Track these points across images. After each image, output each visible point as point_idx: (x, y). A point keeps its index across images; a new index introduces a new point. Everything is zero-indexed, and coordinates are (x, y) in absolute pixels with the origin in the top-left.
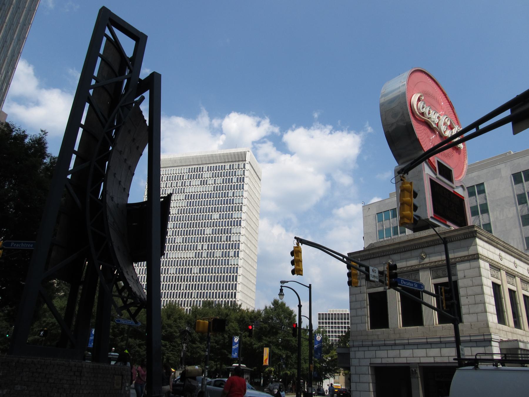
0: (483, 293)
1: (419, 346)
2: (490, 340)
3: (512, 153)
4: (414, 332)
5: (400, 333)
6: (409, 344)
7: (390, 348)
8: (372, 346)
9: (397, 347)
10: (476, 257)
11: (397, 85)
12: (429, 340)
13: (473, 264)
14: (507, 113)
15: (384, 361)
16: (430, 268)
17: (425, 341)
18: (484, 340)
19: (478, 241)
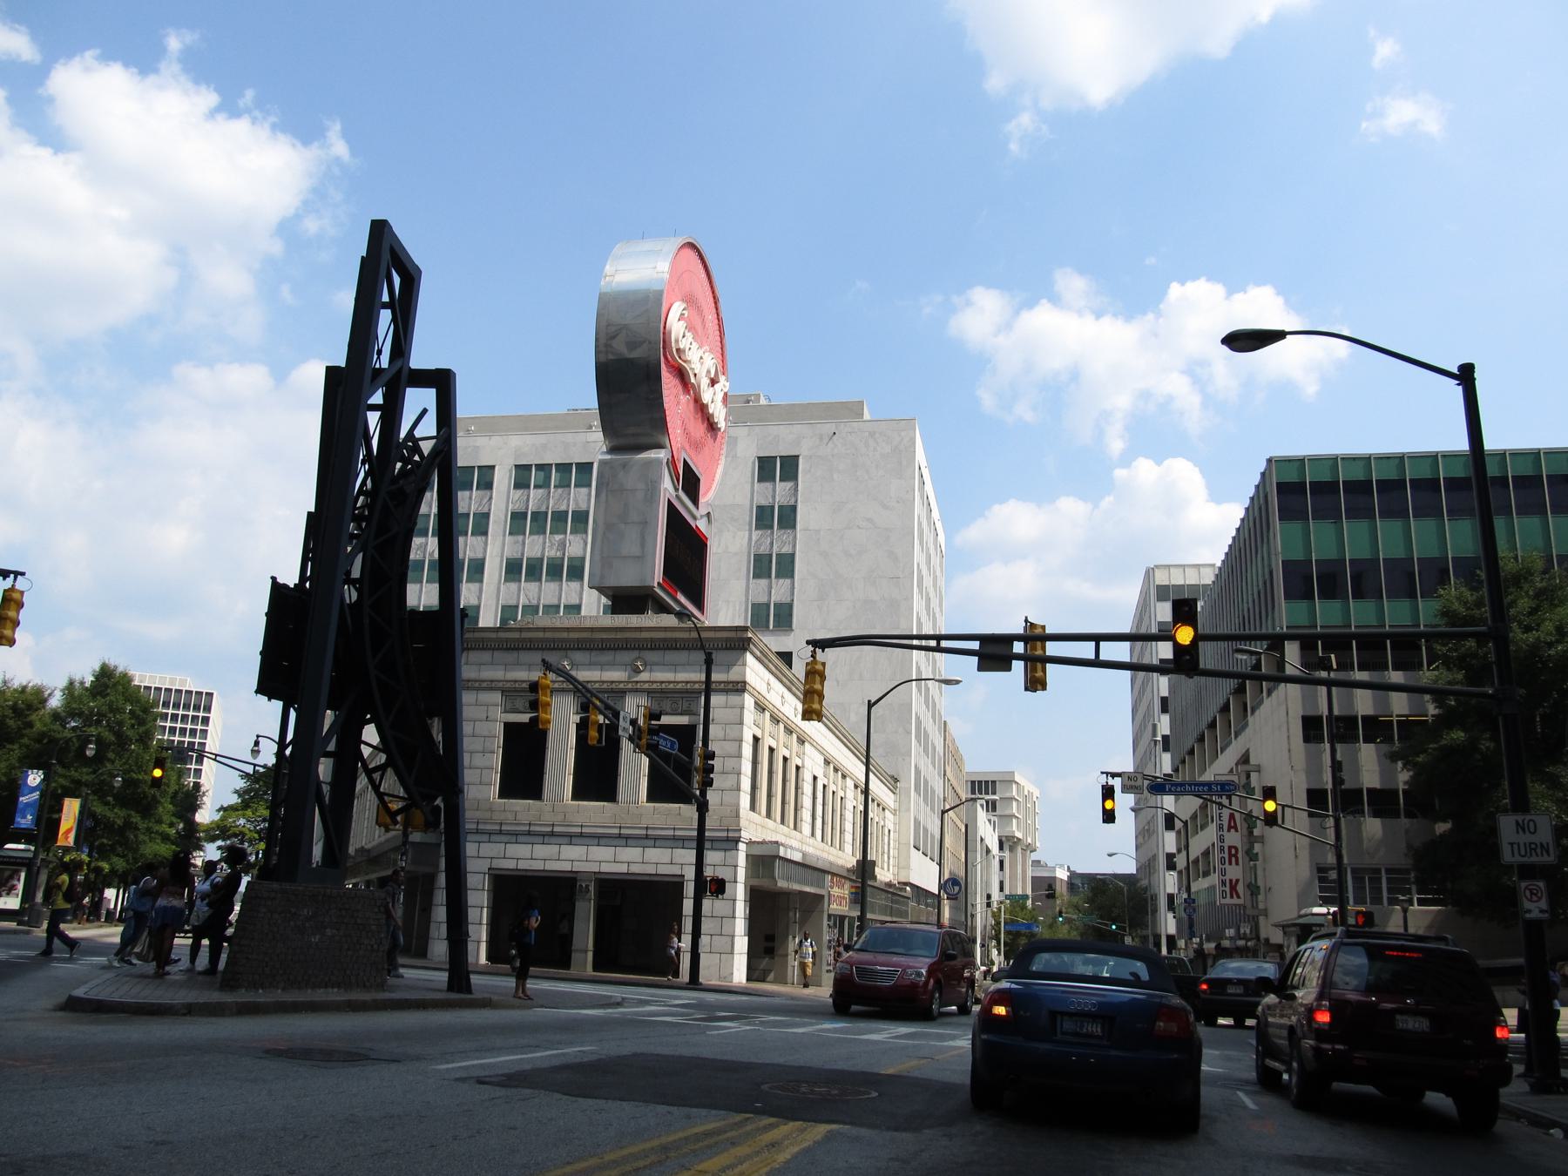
0: (740, 756)
1: (603, 841)
2: (737, 840)
3: (763, 401)
4: (594, 812)
5: (491, 810)
6: (581, 835)
7: (540, 839)
8: (500, 832)
9: (553, 840)
10: (740, 687)
11: (641, 267)
12: (678, 833)
13: (733, 699)
14: (975, 645)
15: (523, 865)
16: (649, 692)
17: (616, 831)
18: (728, 839)
19: (749, 657)
